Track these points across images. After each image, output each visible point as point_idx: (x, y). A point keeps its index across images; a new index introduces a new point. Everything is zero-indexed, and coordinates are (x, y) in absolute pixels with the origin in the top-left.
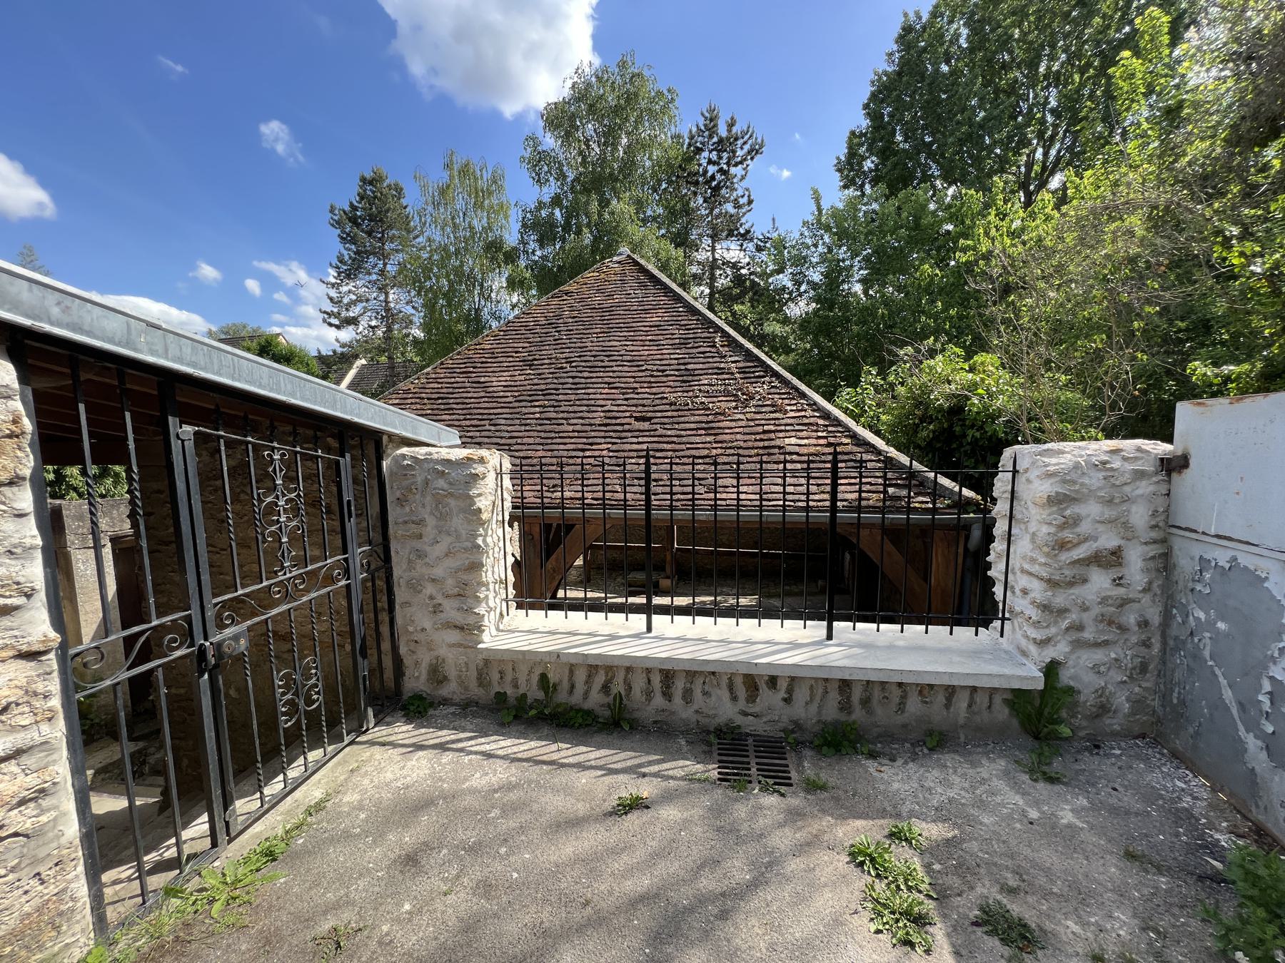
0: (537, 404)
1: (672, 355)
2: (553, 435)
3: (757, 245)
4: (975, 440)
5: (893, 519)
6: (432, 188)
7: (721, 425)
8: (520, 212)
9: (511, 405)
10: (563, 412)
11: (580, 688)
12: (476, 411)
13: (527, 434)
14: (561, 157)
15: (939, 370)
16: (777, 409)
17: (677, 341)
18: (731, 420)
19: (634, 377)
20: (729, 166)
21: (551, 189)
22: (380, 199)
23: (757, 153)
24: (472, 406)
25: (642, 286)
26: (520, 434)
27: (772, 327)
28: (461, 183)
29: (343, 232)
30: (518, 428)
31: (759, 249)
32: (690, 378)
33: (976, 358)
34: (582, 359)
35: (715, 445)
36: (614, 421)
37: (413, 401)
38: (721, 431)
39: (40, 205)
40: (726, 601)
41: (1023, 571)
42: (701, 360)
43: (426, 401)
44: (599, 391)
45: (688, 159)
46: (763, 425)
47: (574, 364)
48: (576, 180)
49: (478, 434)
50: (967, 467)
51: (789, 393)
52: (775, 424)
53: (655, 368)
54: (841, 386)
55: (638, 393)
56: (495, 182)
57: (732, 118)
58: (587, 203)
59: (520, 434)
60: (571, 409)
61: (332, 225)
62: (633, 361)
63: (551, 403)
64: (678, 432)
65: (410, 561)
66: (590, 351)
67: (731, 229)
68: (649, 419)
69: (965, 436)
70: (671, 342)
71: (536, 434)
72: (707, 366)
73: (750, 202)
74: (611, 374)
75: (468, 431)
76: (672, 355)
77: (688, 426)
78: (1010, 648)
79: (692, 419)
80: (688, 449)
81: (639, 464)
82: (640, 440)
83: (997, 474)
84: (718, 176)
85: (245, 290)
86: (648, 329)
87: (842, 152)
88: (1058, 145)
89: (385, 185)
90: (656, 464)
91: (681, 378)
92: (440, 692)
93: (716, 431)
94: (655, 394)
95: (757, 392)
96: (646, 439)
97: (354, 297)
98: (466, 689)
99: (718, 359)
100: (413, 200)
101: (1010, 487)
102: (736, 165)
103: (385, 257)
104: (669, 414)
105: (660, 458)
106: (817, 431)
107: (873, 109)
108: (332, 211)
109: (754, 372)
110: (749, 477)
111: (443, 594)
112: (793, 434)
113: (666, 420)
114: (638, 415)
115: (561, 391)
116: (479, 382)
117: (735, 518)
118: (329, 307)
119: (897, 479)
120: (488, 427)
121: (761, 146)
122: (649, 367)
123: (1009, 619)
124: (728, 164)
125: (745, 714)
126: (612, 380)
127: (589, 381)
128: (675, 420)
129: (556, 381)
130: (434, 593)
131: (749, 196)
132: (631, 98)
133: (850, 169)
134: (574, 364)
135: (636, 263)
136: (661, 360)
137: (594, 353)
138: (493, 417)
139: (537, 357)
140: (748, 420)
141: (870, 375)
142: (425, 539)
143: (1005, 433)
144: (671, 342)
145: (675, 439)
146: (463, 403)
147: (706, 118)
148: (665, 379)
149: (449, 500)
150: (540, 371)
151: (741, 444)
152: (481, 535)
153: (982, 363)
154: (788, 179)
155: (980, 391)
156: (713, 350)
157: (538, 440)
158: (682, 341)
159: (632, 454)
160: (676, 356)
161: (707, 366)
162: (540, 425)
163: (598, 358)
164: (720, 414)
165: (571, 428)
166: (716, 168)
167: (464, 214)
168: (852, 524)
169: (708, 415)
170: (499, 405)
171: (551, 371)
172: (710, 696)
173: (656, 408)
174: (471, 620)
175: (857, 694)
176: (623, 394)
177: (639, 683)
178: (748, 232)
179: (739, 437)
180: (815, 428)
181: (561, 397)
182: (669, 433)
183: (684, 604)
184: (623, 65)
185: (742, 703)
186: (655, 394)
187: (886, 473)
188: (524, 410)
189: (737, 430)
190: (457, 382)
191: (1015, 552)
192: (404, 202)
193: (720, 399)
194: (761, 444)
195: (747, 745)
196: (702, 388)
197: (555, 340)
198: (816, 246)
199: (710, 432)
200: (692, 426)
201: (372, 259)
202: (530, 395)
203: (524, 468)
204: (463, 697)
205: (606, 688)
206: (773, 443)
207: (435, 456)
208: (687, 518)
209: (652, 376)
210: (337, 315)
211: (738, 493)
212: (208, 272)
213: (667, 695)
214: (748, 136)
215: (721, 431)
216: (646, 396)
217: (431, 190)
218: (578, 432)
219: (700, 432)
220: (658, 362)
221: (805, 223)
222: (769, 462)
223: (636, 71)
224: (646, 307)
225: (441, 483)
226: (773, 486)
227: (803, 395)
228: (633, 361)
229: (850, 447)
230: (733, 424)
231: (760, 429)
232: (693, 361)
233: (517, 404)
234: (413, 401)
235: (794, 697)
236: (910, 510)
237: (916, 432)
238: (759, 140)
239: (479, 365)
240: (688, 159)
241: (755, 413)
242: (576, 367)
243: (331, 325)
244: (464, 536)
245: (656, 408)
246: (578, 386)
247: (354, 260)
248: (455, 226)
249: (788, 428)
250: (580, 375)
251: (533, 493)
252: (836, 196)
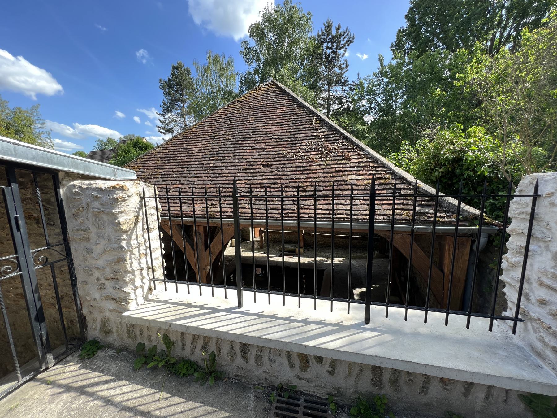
0: (212, 159)
1: (287, 130)
2: (218, 175)
3: (350, 87)
4: (469, 178)
5: (419, 228)
6: (201, 69)
7: (311, 168)
8: (239, 77)
9: (199, 160)
10: (225, 163)
11: (189, 346)
12: (182, 163)
13: (204, 175)
14: (258, 50)
15: (447, 136)
16: (344, 157)
17: (292, 122)
18: (317, 165)
19: (265, 143)
20: (337, 50)
21: (254, 66)
22: (180, 76)
23: (351, 42)
24: (181, 161)
25: (277, 95)
26: (201, 175)
27: (359, 127)
28: (214, 66)
29: (165, 91)
30: (200, 172)
31: (351, 90)
32: (296, 142)
33: (470, 129)
34: (240, 134)
35: (306, 180)
36: (251, 167)
37: (153, 159)
38: (311, 172)
39: (59, 91)
40: (327, 261)
41: (542, 284)
42: (303, 132)
43: (159, 159)
44: (245, 151)
45: (317, 47)
46: (336, 168)
47: (235, 137)
48: (265, 61)
49: (180, 176)
50: (463, 193)
51: (353, 148)
52: (343, 167)
53: (277, 137)
54: (389, 152)
55: (266, 152)
56: (229, 65)
57: (339, 26)
58: (269, 71)
59: (201, 175)
60: (229, 161)
61: (161, 88)
62: (267, 134)
63: (220, 158)
64: (286, 173)
65: (84, 256)
66: (245, 130)
67: (339, 81)
68: (271, 165)
69: (462, 175)
70: (288, 123)
71: (209, 175)
72: (306, 135)
73: (347, 66)
74: (253, 142)
75: (176, 174)
76: (287, 130)
77: (291, 169)
78: (522, 344)
79: (295, 165)
80: (290, 182)
81: (261, 192)
82: (264, 177)
83: (512, 198)
84: (332, 55)
85: (134, 121)
86: (276, 117)
87: (394, 40)
88: (508, 30)
89: (183, 69)
90: (270, 192)
91: (291, 142)
92: (108, 339)
93: (308, 172)
94: (275, 152)
95: (334, 148)
96: (267, 177)
97: (170, 120)
98: (122, 339)
99: (313, 131)
100: (194, 75)
101: (529, 210)
102: (340, 49)
103: (183, 102)
104: (282, 162)
105: (273, 188)
106: (369, 171)
107: (409, 17)
108: (160, 82)
109: (333, 137)
110: (324, 200)
111: (104, 278)
112: (354, 172)
113: (280, 166)
114: (264, 163)
115: (226, 152)
116: (187, 149)
117: (313, 226)
118: (160, 124)
119: (421, 201)
120: (185, 172)
121: (353, 39)
122: (274, 137)
123: (521, 320)
124: (336, 49)
125: (300, 378)
126: (254, 145)
127: (241, 145)
128: (285, 166)
129: (224, 146)
130: (100, 277)
131: (346, 64)
132: (289, 19)
133: (398, 47)
134: (235, 137)
135: (275, 84)
136: (281, 133)
137: (246, 131)
138: (189, 166)
139: (217, 134)
140: (327, 165)
141: (406, 144)
142: (92, 241)
143: (490, 173)
144: (288, 123)
145: (283, 177)
146: (176, 160)
147: (326, 26)
148: (282, 143)
149: (103, 216)
150: (218, 142)
151: (322, 179)
152: (124, 239)
153: (475, 132)
154: (366, 59)
155: (473, 148)
156: (311, 126)
157: (209, 179)
158: (294, 122)
159: (257, 186)
160: (290, 130)
161: (306, 135)
162: (212, 170)
163: (248, 134)
164: (311, 162)
165: (227, 171)
166: (331, 51)
167: (216, 80)
168: (389, 231)
169: (304, 163)
170: (194, 160)
171: (223, 141)
172: (274, 362)
173: (275, 160)
174: (121, 295)
175: (386, 377)
176: (258, 152)
177: (225, 349)
178: (346, 81)
179: (320, 175)
180: (368, 169)
181: (225, 155)
182: (280, 173)
183: (306, 262)
184: (286, 3)
185: (297, 370)
186: (275, 152)
187: (415, 197)
188: (205, 162)
189: (320, 171)
190: (177, 149)
191: (531, 265)
192: (191, 76)
193: (312, 153)
194: (333, 179)
195: (298, 406)
196: (302, 147)
197: (228, 125)
198: (380, 85)
199: (304, 172)
200: (294, 169)
201: (178, 103)
202: (210, 154)
203: (182, 194)
204: (120, 344)
205: (204, 348)
206: (341, 178)
207: (94, 186)
208: (279, 224)
209: (275, 142)
210: (164, 128)
211: (315, 209)
212: (120, 114)
213: (245, 359)
214: (346, 34)
215: (311, 172)
216: (271, 153)
217: (200, 69)
218: (231, 173)
219: (298, 173)
220: (280, 134)
221: (374, 74)
222: (337, 190)
223: (293, 5)
224: (277, 106)
225: (96, 204)
226: (342, 206)
227: (362, 149)
228: (267, 134)
229: (390, 180)
230: (318, 167)
231: (334, 170)
232: (299, 132)
233: (203, 159)
234: (153, 159)
235: (336, 371)
236: (435, 223)
237: (431, 173)
238: (352, 36)
239: (189, 140)
240: (317, 47)
241: (331, 160)
242: (236, 138)
243: (161, 132)
244: (113, 240)
245: (275, 160)
246: (235, 149)
247: (170, 103)
248: (212, 86)
249: (351, 169)
250: (237, 143)
251: (200, 209)
252: (389, 59)
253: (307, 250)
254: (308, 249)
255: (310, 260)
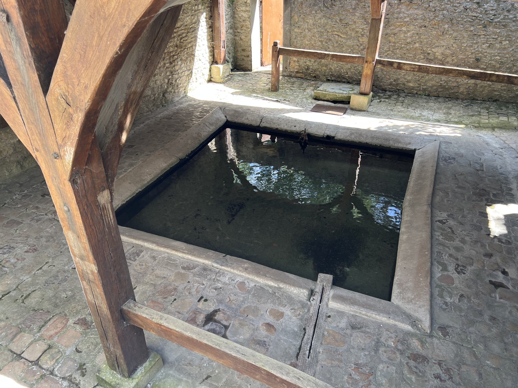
253: (376, 101)
254: (380, 97)
255: (383, 125)
